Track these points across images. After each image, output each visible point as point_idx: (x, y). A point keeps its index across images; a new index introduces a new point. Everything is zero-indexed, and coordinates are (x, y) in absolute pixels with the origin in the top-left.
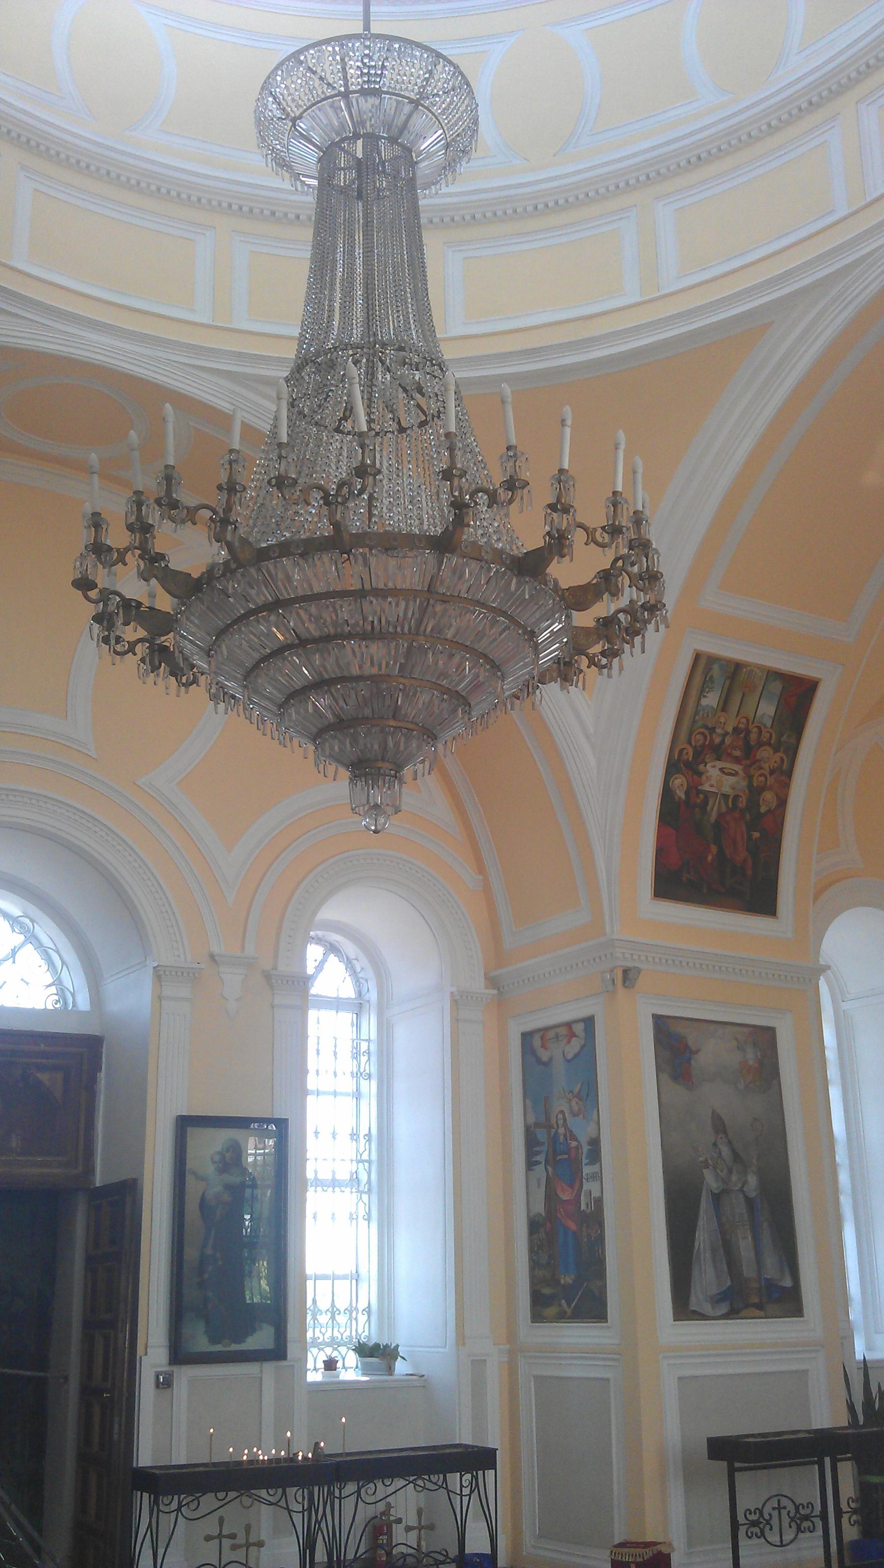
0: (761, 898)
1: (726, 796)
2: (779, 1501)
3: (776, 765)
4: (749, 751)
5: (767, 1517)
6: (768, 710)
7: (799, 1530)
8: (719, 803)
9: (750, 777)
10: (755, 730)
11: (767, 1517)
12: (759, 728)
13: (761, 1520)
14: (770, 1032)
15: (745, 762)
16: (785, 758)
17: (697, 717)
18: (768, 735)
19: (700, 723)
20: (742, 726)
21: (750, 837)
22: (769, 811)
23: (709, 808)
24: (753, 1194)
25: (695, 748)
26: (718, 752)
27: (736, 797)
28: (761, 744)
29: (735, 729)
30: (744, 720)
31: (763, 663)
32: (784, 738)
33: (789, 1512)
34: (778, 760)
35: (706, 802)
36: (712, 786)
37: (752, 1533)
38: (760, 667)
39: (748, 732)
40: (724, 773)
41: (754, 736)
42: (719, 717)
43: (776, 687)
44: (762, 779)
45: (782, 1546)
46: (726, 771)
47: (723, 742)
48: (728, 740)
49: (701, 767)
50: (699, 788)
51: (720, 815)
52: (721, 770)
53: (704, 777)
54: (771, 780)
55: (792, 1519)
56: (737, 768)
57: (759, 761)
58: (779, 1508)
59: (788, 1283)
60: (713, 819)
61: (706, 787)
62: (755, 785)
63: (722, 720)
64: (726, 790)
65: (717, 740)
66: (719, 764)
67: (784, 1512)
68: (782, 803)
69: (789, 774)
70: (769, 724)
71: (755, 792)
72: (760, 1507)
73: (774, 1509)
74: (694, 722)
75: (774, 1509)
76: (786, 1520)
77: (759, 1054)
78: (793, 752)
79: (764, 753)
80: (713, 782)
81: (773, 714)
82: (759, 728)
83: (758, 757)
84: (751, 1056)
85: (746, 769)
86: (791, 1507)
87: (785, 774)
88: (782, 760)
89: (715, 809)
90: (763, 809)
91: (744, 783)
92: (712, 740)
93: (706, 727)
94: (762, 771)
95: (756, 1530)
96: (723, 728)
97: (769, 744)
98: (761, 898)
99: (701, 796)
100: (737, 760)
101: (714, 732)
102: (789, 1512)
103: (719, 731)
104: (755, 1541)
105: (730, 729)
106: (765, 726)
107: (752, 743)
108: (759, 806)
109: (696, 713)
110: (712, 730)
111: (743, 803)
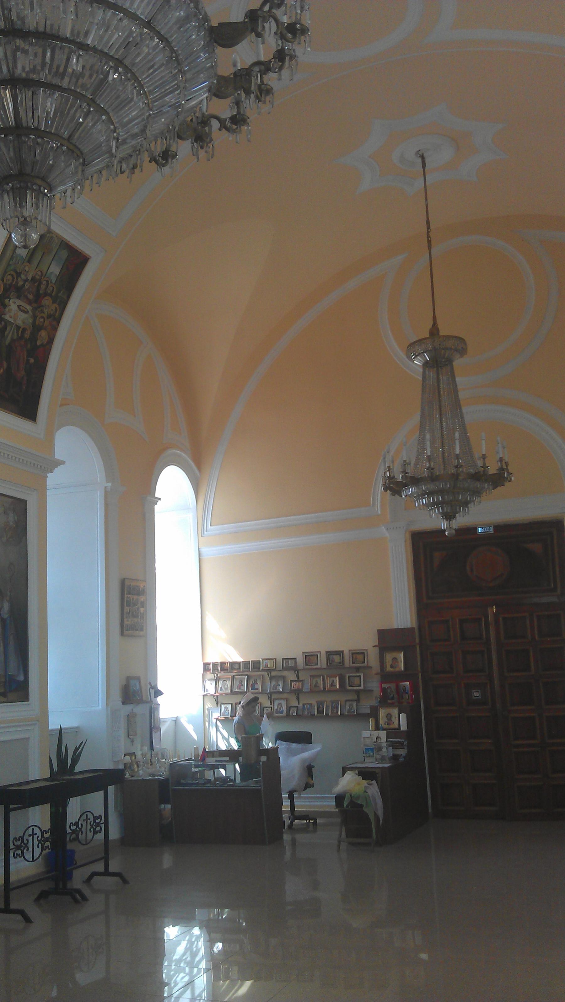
0: (27, 408)
1: (18, 327)
2: (33, 829)
3: (52, 313)
4: (38, 298)
5: (26, 842)
6: (55, 270)
7: (22, 838)
8: (13, 332)
9: (35, 317)
10: (45, 282)
11: (26, 842)
12: (47, 281)
13: (22, 845)
14: (24, 503)
15: (35, 305)
16: (58, 308)
17: (11, 262)
18: (52, 288)
19: (12, 267)
20: (38, 277)
21: (28, 361)
22: (42, 345)
23: (6, 333)
24: (5, 616)
25: (5, 285)
26: (19, 292)
27: (24, 330)
28: (46, 294)
29: (33, 279)
30: (39, 273)
31: (61, 234)
32: (60, 294)
33: (38, 837)
34: (54, 309)
35: (5, 328)
36: (11, 317)
37: (17, 854)
38: (58, 237)
39: (40, 283)
40: (20, 309)
41: (43, 287)
42: (25, 266)
43: (64, 254)
44: (42, 320)
45: (33, 861)
46: (22, 308)
47: (23, 286)
48: (27, 285)
49: (7, 301)
50: (3, 316)
51: (13, 340)
52: (18, 306)
53: (7, 310)
54: (47, 323)
55: (40, 842)
56: (29, 308)
57: (43, 306)
58: (33, 835)
59: (21, 678)
60: (7, 343)
61: (7, 317)
62: (37, 324)
63: (27, 269)
64: (19, 322)
65: (20, 283)
66: (19, 302)
67: (35, 837)
68: (51, 341)
69: (58, 320)
70: (54, 281)
71: (36, 328)
72: (22, 835)
73: (29, 836)
74: (9, 265)
75: (29, 836)
76: (36, 842)
77: (16, 518)
78: (63, 305)
79: (47, 301)
80: (12, 314)
81: (58, 273)
82: (47, 281)
83: (43, 303)
84: (12, 518)
85: (35, 309)
86: (39, 834)
87: (56, 319)
88: (56, 309)
89: (10, 335)
90: (39, 343)
91: (31, 321)
92: (17, 282)
93: (15, 271)
94: (42, 315)
95: (19, 852)
96: (26, 276)
97: (50, 295)
98: (27, 408)
99: (3, 323)
100: (30, 303)
101: (20, 276)
102: (38, 837)
103: (23, 277)
104: (19, 859)
105: (30, 278)
106: (51, 282)
107: (41, 292)
108: (36, 340)
109: (12, 258)
110: (19, 275)
111: (27, 335)
